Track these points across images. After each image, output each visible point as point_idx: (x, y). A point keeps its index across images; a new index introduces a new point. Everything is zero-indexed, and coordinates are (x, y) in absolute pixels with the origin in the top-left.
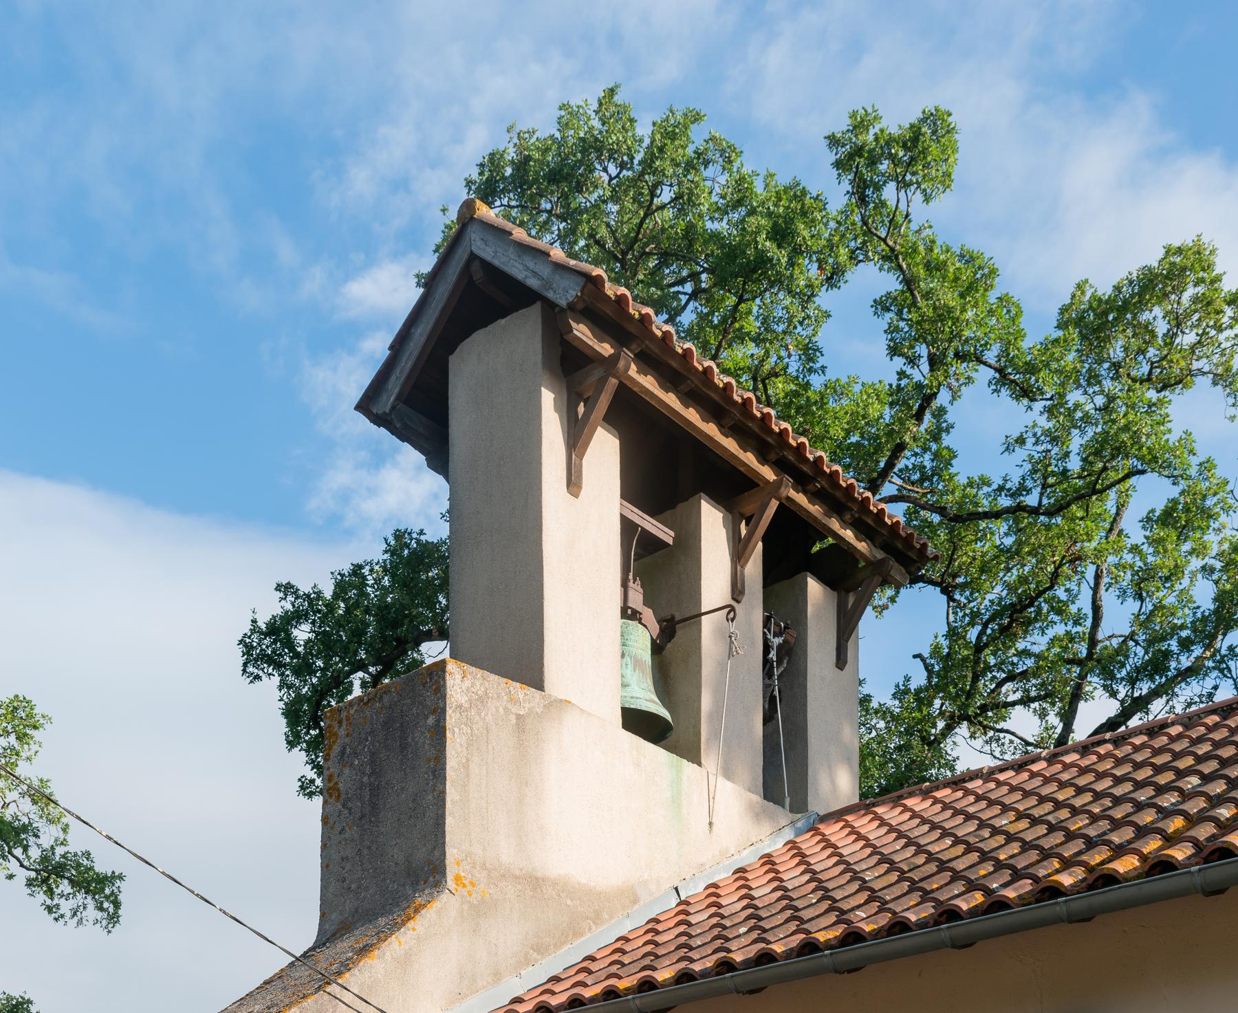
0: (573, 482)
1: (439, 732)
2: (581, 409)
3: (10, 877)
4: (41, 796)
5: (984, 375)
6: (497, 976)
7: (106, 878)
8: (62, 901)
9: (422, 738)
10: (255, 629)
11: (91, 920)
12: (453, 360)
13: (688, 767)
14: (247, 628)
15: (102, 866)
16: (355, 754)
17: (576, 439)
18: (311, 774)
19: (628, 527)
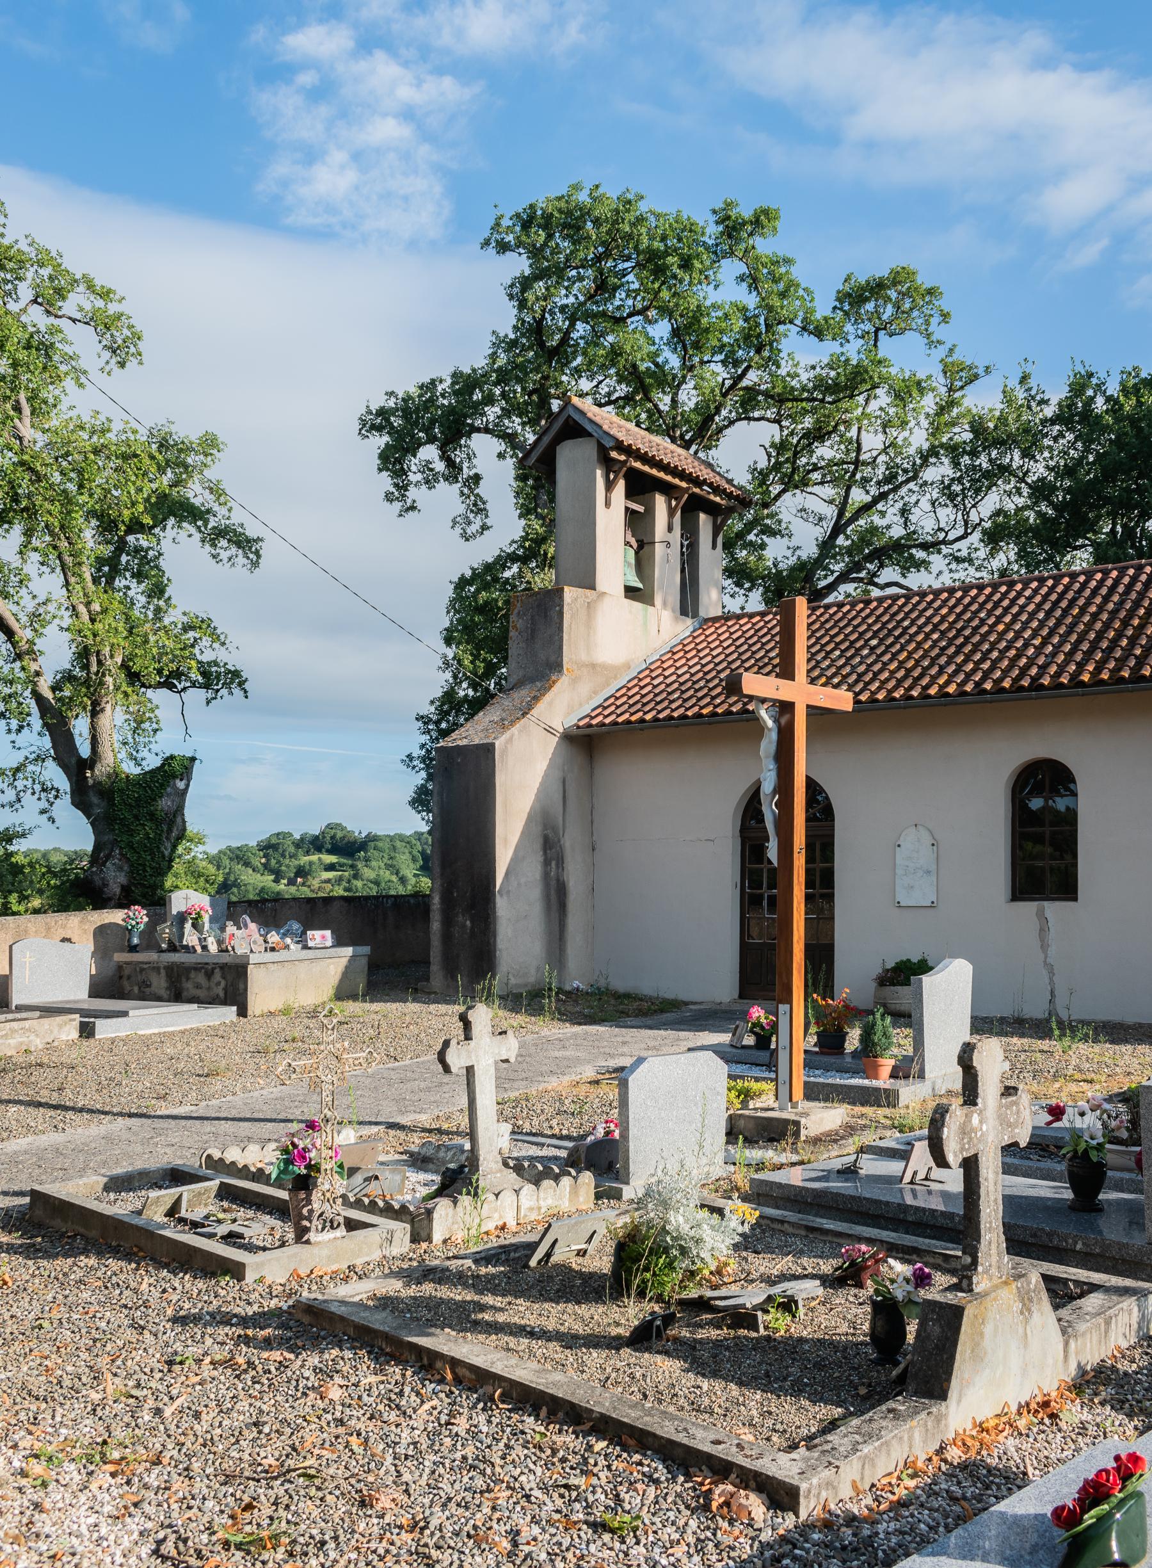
0: (608, 504)
1: (561, 614)
2: (612, 476)
3: (190, 536)
4: (216, 490)
5: (794, 330)
6: (581, 705)
7: (254, 541)
8: (222, 551)
9: (553, 614)
10: (370, 412)
11: (241, 564)
12: (558, 448)
13: (650, 608)
14: (363, 411)
15: (251, 533)
16: (524, 614)
17: (609, 486)
18: (393, 490)
19: (627, 509)
